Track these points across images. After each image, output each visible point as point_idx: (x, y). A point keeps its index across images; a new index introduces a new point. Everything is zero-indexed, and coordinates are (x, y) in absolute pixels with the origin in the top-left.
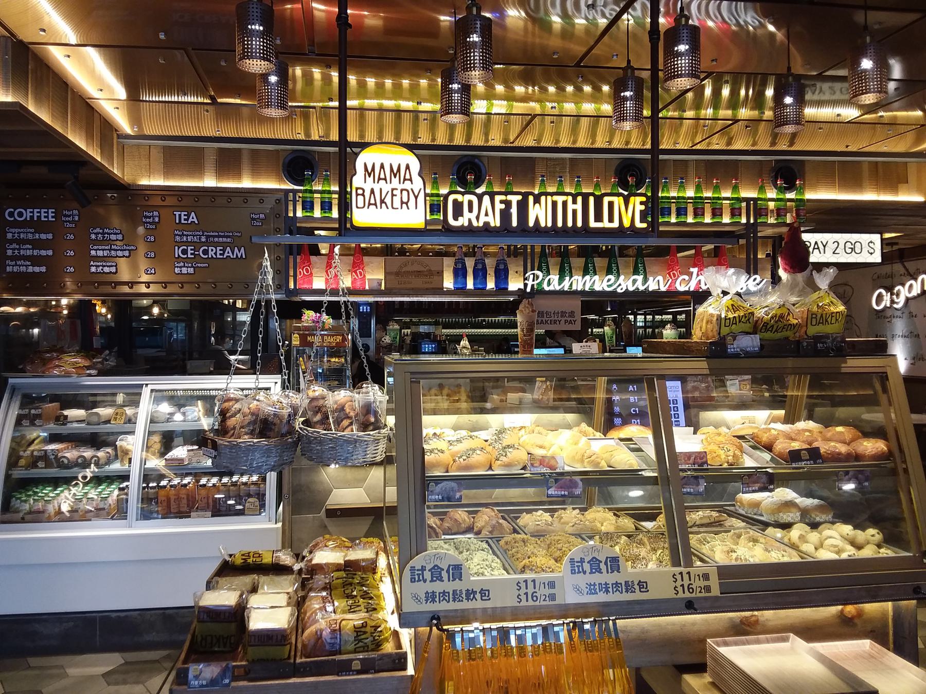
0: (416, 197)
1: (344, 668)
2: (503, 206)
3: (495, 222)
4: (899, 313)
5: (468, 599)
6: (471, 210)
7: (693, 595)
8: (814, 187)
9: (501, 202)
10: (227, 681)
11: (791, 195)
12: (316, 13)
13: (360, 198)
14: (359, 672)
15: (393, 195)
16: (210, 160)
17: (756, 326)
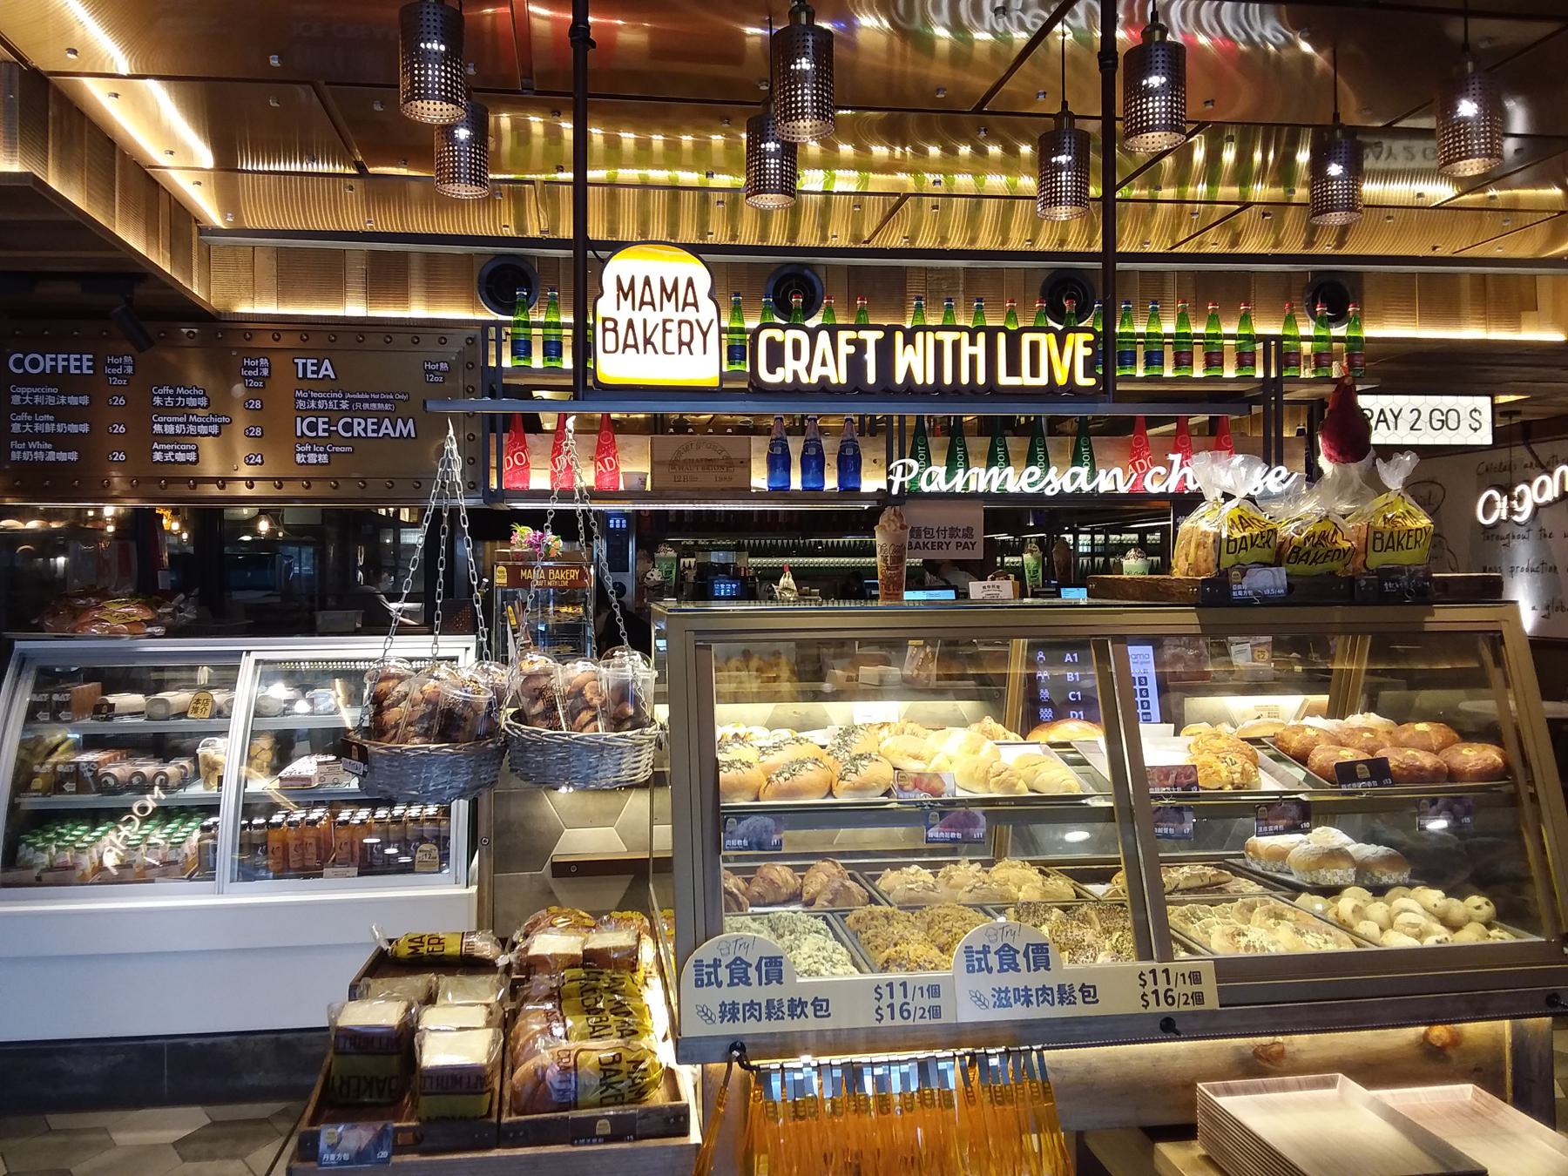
0: (705, 335)
1: (582, 1131)
2: (852, 349)
3: (839, 376)
4: (1522, 531)
5: (792, 1015)
6: (797, 356)
7: (1174, 1008)
8: (1379, 317)
9: (849, 342)
10: (384, 1154)
11: (1339, 331)
12: (535, 22)
13: (610, 336)
14: (608, 1139)
15: (665, 331)
16: (356, 271)
17: (1280, 553)
